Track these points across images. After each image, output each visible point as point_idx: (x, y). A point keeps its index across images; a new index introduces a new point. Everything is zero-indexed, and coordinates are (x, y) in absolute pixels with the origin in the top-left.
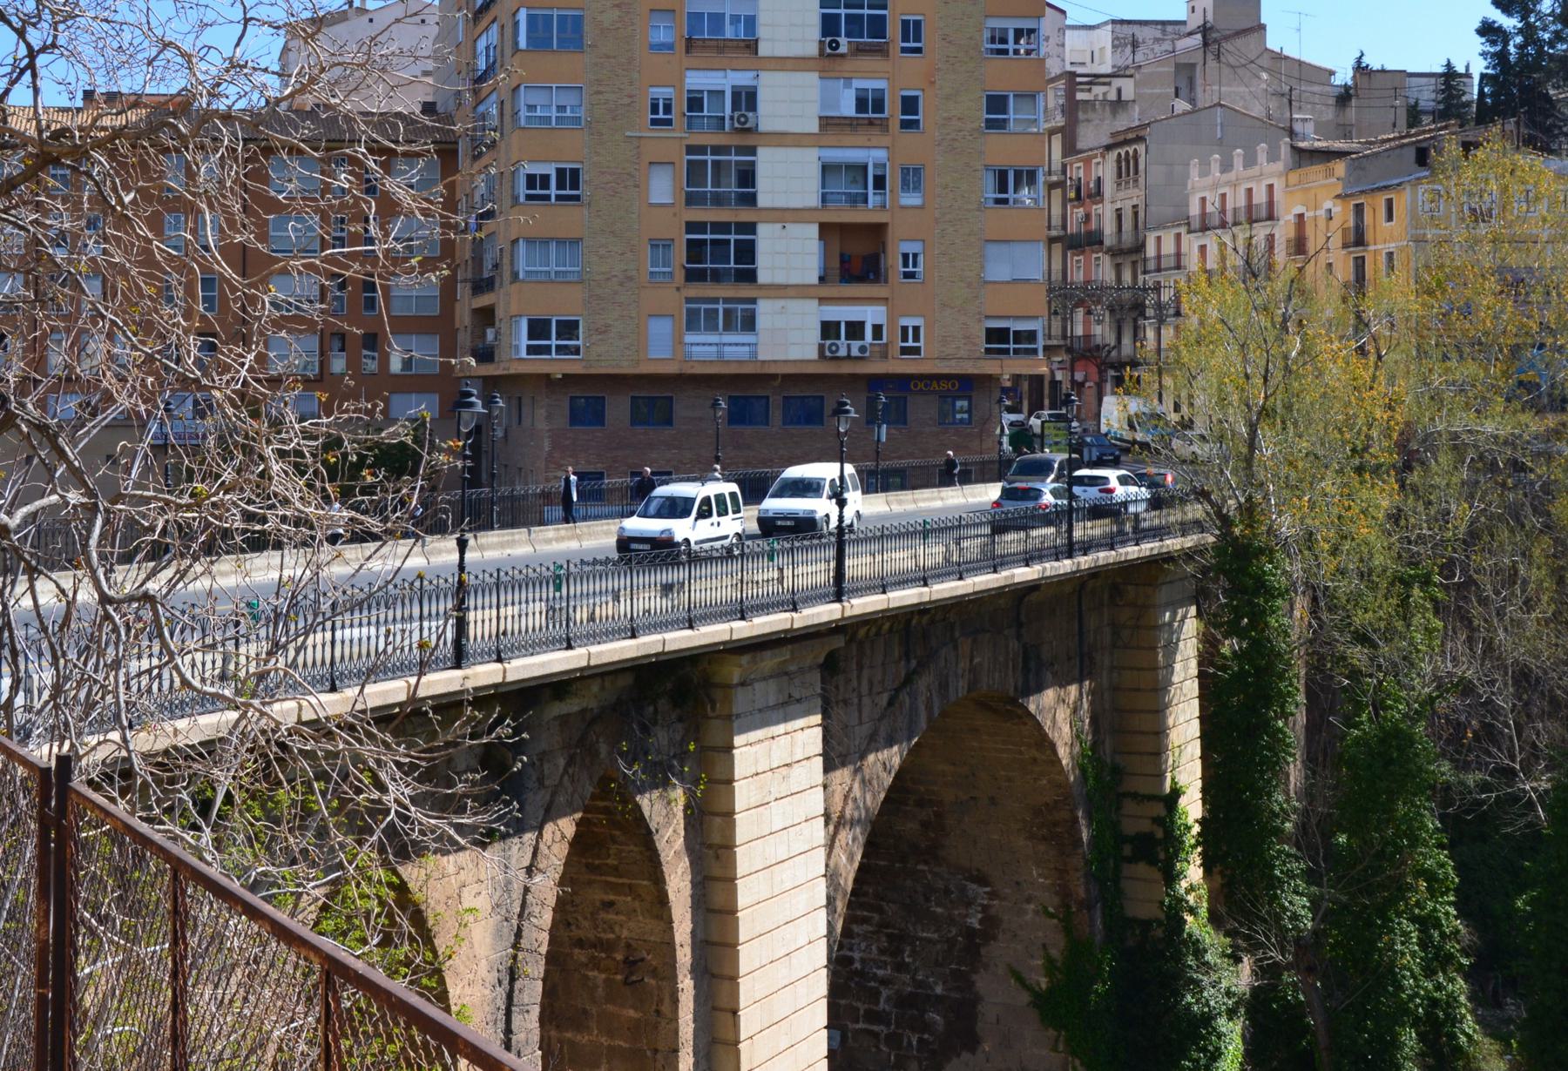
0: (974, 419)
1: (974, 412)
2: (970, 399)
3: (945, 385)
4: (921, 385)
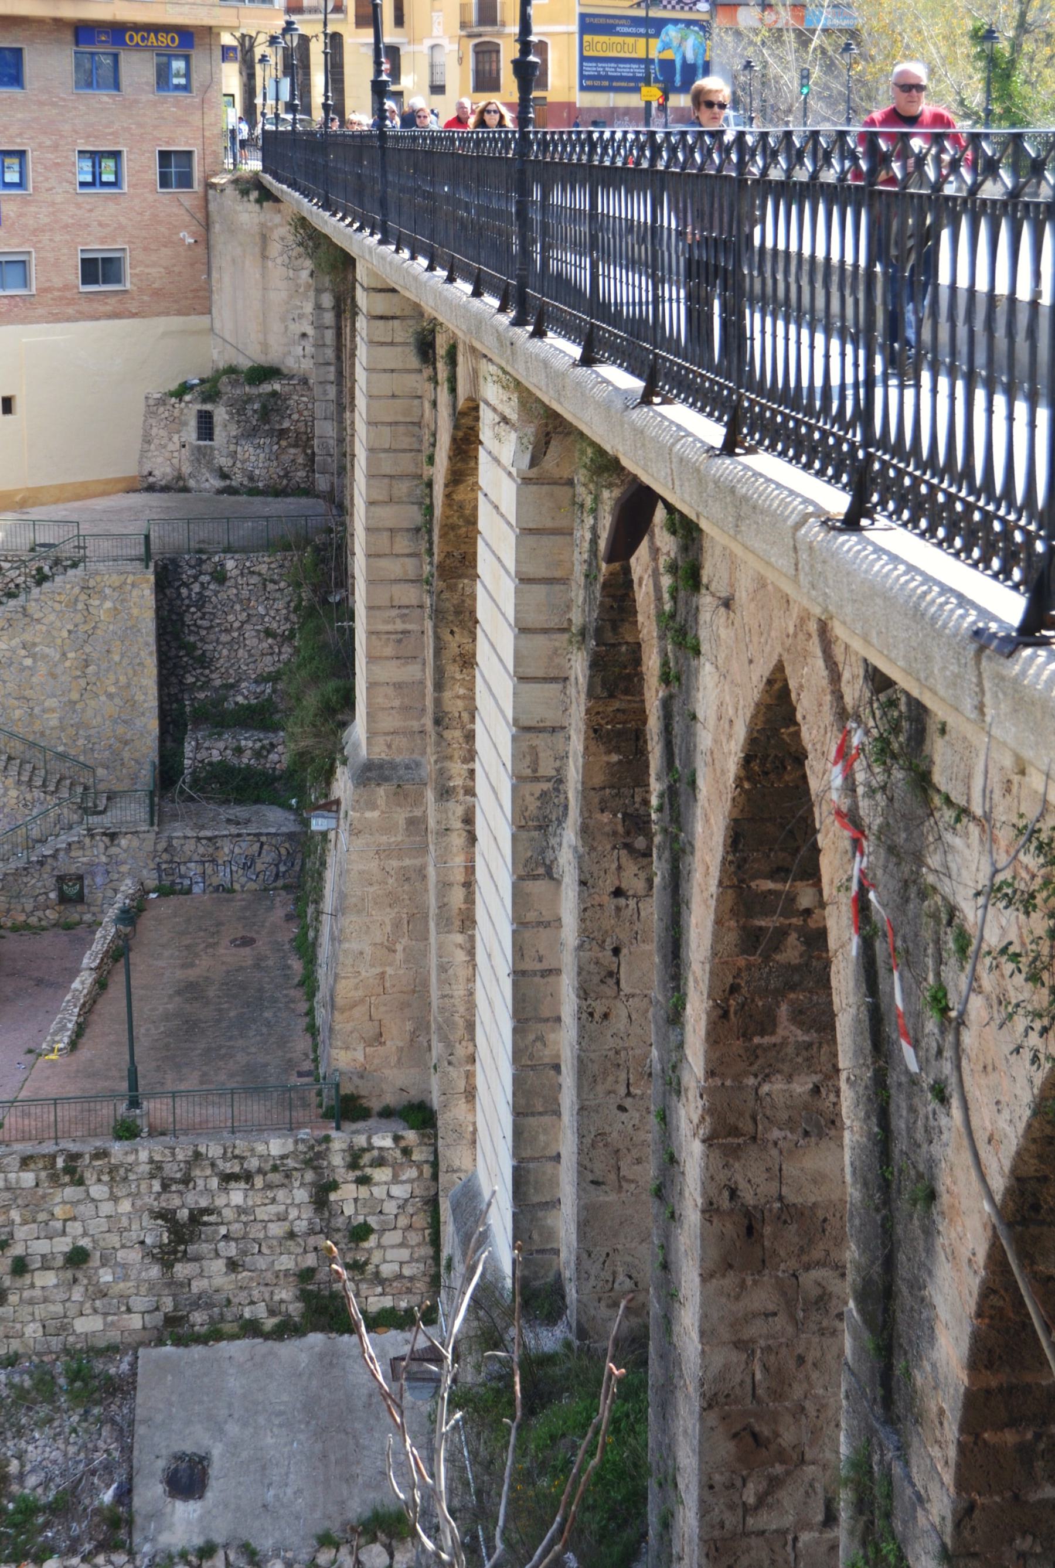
0: (195, 84)
1: (194, 76)
2: (187, 58)
3: (164, 39)
4: (137, 38)
